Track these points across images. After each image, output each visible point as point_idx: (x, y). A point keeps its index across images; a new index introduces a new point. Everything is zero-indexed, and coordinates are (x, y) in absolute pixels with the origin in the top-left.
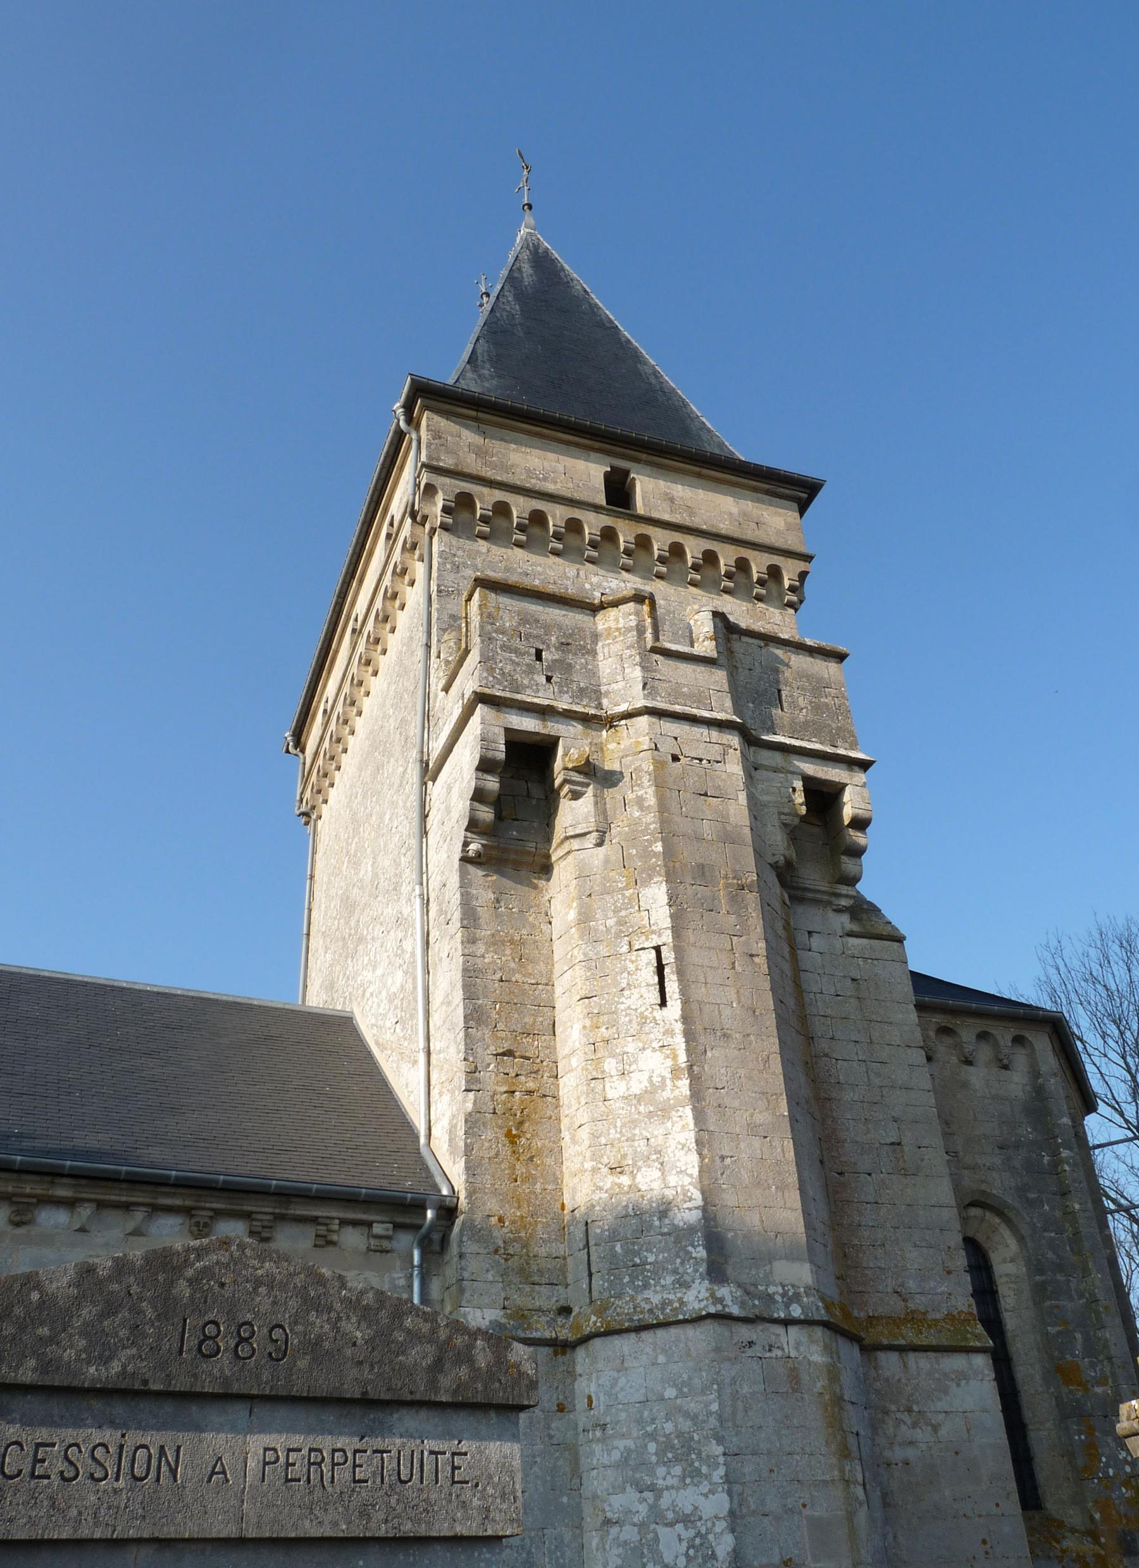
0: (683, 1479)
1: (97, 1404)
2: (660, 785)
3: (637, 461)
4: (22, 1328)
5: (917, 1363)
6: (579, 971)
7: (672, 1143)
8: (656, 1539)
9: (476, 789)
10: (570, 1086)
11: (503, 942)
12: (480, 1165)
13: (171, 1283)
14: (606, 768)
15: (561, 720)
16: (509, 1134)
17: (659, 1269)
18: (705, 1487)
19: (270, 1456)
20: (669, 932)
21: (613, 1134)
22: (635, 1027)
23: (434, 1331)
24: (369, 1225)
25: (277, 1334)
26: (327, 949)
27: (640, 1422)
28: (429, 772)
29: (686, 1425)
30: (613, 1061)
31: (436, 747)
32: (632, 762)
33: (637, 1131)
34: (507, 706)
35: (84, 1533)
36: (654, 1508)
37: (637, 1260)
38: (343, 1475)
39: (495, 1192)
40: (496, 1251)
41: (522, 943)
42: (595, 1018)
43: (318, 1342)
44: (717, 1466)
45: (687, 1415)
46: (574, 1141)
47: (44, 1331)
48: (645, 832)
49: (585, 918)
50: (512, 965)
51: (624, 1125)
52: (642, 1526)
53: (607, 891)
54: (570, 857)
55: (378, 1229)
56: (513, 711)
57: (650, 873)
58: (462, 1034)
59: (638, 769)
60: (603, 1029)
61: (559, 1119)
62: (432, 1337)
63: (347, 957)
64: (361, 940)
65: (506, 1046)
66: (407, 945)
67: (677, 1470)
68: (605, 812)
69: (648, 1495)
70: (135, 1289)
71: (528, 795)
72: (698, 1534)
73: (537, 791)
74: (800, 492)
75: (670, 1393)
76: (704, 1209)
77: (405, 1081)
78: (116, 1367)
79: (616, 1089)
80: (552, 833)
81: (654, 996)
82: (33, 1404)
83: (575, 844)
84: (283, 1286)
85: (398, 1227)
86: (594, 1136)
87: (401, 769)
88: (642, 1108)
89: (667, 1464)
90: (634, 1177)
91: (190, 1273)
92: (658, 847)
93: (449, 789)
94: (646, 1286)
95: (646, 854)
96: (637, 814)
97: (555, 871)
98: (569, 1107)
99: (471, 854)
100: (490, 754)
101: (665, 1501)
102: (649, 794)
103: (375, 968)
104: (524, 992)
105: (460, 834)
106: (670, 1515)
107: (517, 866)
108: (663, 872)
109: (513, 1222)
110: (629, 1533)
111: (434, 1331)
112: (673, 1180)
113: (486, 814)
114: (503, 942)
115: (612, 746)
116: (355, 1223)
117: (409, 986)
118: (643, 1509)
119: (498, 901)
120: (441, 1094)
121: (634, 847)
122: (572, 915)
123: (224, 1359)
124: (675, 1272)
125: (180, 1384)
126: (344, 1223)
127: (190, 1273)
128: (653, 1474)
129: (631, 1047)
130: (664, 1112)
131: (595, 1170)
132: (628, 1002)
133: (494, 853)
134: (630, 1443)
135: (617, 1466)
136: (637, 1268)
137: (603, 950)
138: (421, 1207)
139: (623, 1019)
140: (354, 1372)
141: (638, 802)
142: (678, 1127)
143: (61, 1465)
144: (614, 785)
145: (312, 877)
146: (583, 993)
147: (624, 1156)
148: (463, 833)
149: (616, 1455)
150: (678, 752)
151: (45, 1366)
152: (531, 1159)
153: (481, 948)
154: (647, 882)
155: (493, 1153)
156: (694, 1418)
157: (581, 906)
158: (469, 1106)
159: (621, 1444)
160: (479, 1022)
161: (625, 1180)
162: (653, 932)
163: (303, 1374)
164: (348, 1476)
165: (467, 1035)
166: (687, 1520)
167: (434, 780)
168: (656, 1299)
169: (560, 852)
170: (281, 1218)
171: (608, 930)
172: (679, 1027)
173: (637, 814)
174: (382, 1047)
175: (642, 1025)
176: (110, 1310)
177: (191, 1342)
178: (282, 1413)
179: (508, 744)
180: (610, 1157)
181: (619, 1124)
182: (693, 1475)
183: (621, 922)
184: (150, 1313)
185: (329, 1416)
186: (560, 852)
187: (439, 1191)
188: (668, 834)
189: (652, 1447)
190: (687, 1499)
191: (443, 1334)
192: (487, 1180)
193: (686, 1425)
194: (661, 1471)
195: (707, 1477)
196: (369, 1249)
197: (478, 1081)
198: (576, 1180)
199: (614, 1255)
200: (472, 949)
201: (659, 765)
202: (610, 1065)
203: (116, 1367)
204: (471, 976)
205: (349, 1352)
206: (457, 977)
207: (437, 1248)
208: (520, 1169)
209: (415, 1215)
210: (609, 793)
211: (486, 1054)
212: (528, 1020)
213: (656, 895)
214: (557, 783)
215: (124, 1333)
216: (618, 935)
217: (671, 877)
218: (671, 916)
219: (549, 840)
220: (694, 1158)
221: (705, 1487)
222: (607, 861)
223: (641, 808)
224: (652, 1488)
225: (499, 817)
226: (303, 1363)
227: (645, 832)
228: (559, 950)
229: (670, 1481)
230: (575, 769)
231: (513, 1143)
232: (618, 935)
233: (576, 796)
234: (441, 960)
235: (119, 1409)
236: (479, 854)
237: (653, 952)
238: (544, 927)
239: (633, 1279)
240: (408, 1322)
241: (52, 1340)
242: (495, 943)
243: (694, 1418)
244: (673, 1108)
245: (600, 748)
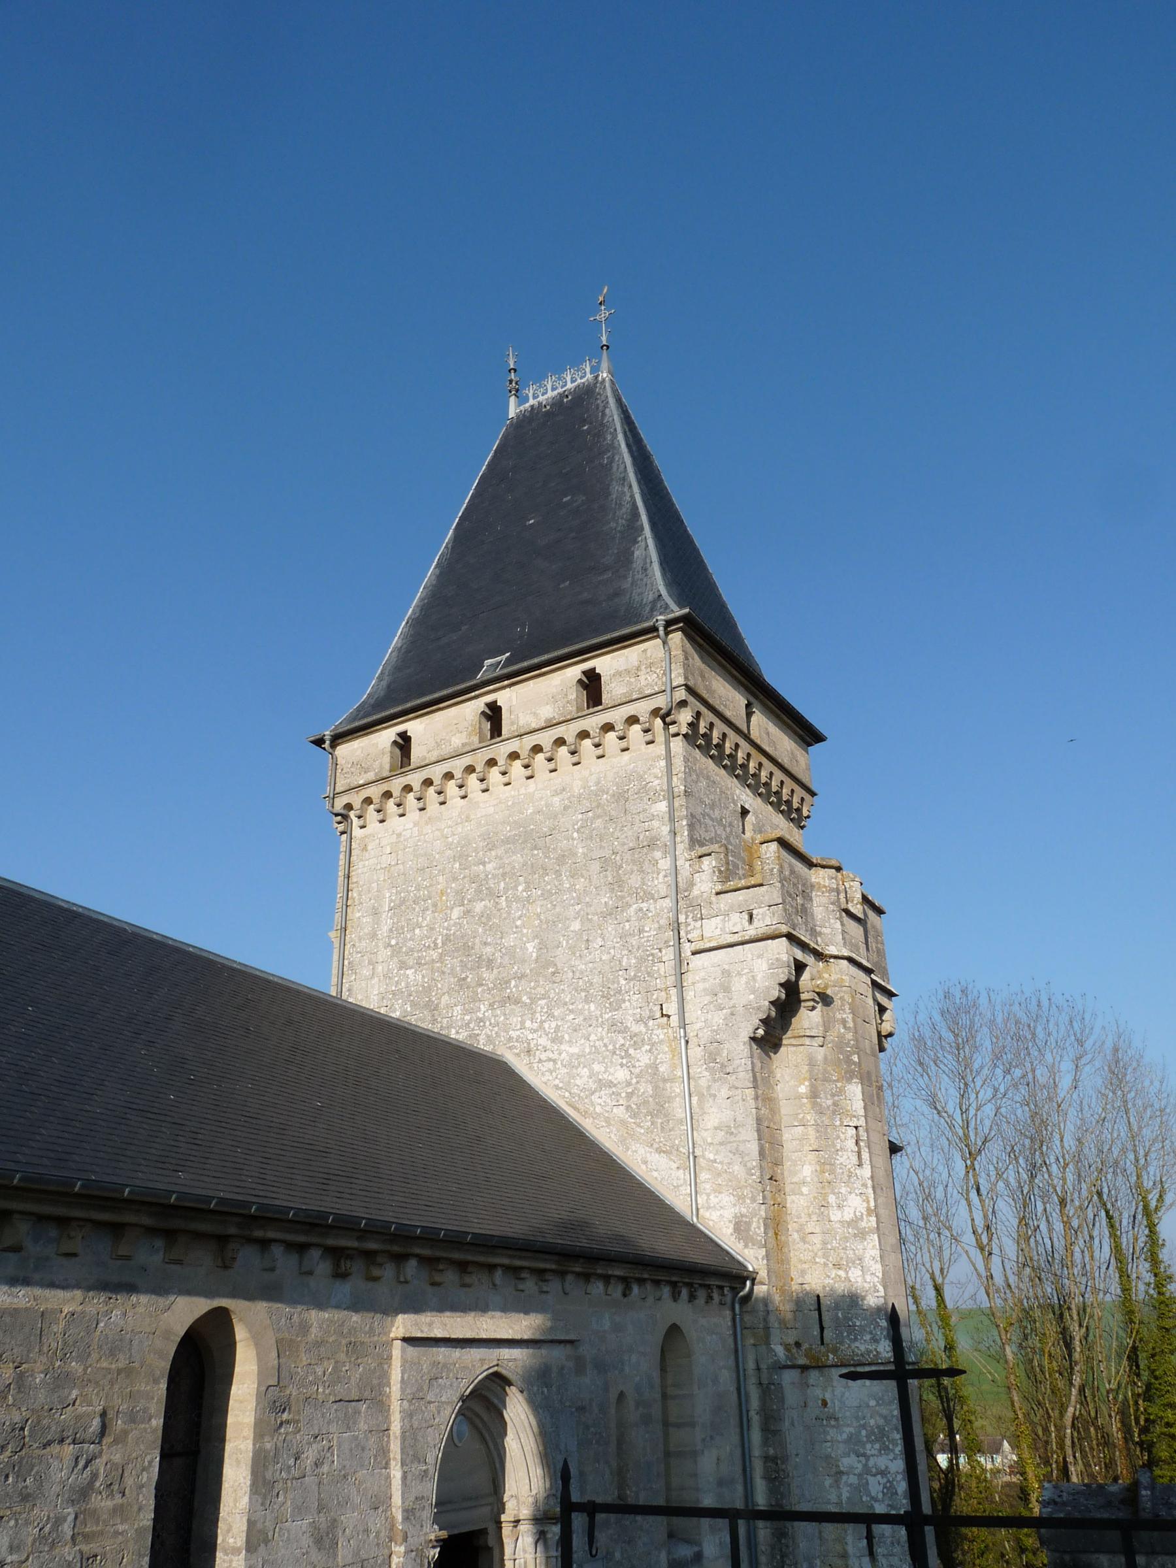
0: (880, 1451)
3: (761, 702)
5: (1109, 1465)
7: (867, 1255)
8: (867, 1483)
17: (863, 1329)
18: (891, 1456)
21: (834, 1244)
22: (845, 1178)
27: (857, 1418)
29: (881, 1422)
36: (865, 1465)
44: (897, 1445)
45: (881, 1416)
48: (848, 1045)
52: (860, 1476)
67: (877, 1446)
69: (862, 1459)
72: (888, 1481)
74: (808, 735)
75: (872, 1403)
76: (884, 1297)
79: (835, 1215)
81: (855, 1160)
83: (807, 1041)
86: (825, 1243)
89: (872, 1442)
90: (847, 1273)
94: (856, 1339)
97: (782, 1049)
101: (871, 1463)
106: (874, 1470)
110: (853, 1479)
112: (868, 1278)
118: (860, 1466)
124: (871, 1333)
128: (864, 1448)
130: (862, 1235)
131: (825, 1265)
132: (842, 1160)
134: (852, 1430)
135: (845, 1442)
136: (851, 1329)
142: (870, 1246)
146: (815, 1147)
149: (845, 1436)
154: (849, 1080)
156: (885, 1418)
159: (847, 1430)
161: (842, 1273)
166: (883, 1473)
168: (863, 1348)
169: (793, 1041)
172: (870, 1183)
175: (849, 1176)
182: (885, 1449)
183: (835, 1104)
189: (864, 1433)
190: (882, 1462)
193: (881, 1422)
194: (869, 1446)
195: (893, 1451)
199: (838, 1318)
202: (832, 1199)
220: (879, 1266)
221: (891, 1456)
223: (845, 1027)
224: (864, 1455)
227: (848, 1045)
229: (873, 1452)
239: (849, 1334)
243: (885, 1418)
244: (868, 1233)
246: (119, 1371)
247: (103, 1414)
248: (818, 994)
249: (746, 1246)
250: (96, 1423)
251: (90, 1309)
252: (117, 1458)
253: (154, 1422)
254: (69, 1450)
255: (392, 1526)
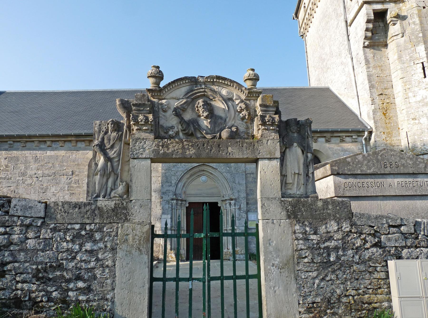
1: (370, 176)
2: (420, 17)
4: (356, 165)
6: (399, 72)
9: (366, 28)
10: (399, 100)
11: (377, 67)
12: (377, 121)
13: (377, 157)
14: (403, 15)
15: (388, 3)
16: (384, 113)
19: (398, 183)
20: (426, 58)
21: (413, 111)
22: (417, 84)
23: (424, 161)
24: (352, 136)
25: (396, 163)
26: (315, 71)
28: (348, 25)
30: (411, 93)
31: (350, 18)
32: (411, 12)
33: (419, 110)
34: (372, 3)
35: (372, 195)
37: (421, 139)
38: (411, 185)
39: (382, 127)
40: (384, 140)
41: (382, 66)
42: (405, 83)
43: (404, 164)
46: (401, 113)
47: (360, 166)
48: (416, 31)
49: (400, 57)
50: (380, 72)
51: (416, 108)
53: (405, 49)
54: (394, 41)
55: (354, 137)
56: (375, 4)
57: (419, 42)
58: (369, 91)
59: (413, 13)
60: (408, 86)
61: (396, 108)
62: (424, 162)
63: (324, 73)
64: (328, 68)
65: (381, 93)
66: (346, 69)
68: (403, 28)
70: (372, 158)
71: (379, 26)
73: (381, 24)
77: (352, 104)
78: (372, 170)
79: (412, 100)
80: (387, 35)
82: (360, 176)
83: (395, 38)
84: (396, 156)
85: (358, 136)
87: (336, 23)
88: (420, 104)
91: (380, 155)
92: (421, 35)
93: (356, 28)
95: (417, 37)
96: (413, 26)
97: (389, 45)
98: (399, 105)
99: (366, 45)
100: (369, 18)
102: (417, 21)
103: (335, 75)
104: (384, 79)
105: (363, 41)
107: (378, 46)
108: (423, 42)
109: (387, 133)
111: (424, 161)
113: (369, 34)
114: (377, 67)
115: (404, 8)
116: (348, 136)
117: (348, 80)
119: (374, 56)
120: (363, 105)
121: (413, 36)
122: (396, 57)
123: (389, 168)
125: (383, 172)
126: (346, 136)
127: (380, 155)
129: (416, 89)
131: (408, 120)
132: (414, 78)
133: (372, 44)
137: (406, 65)
138: (364, 132)
139: (413, 82)
140: (411, 169)
141: (414, 23)
143: (367, 185)
144: (405, 19)
145: (307, 52)
147: (416, 116)
148: (363, 40)
150: (424, 6)
151: (361, 171)
152: (390, 118)
153: (371, 69)
154: (418, 45)
155: (380, 118)
157: (398, 54)
158: (373, 108)
160: (373, 88)
162: (421, 59)
163: (402, 170)
164: (412, 185)
165: (370, 91)
167: (350, 26)
169: (391, 40)
170: (332, 137)
171: (407, 60)
173: (413, 26)
174: (341, 95)
176: (369, 162)
177: (383, 166)
178: (399, 176)
179: (374, 14)
180: (412, 116)
181: (414, 108)
183: (410, 57)
184: (375, 162)
185: (407, 176)
186: (391, 40)
187: (367, 128)
188: (423, 31)
191: (426, 162)
192: (380, 124)
196: (352, 141)
197: (374, 102)
198: (402, 122)
200: (369, 70)
201: (419, 11)
202: (410, 94)
203: (372, 170)
204: (369, 77)
205: (409, 166)
206: (366, 77)
207: (368, 140)
208: (387, 121)
209: (359, 132)
210: (404, 22)
211: (375, 95)
212: (386, 85)
213: (421, 49)
214: (388, 22)
215: (372, 165)
216: (410, 61)
217: (425, 43)
218: (426, 53)
219: (387, 37)
222: (405, 41)
223: (415, 24)
225: (372, 34)
226: (402, 168)
228: (392, 66)
230: (394, 17)
231: (385, 115)
232: (410, 61)
233: (394, 24)
234: (359, 73)
235: (373, 176)
236: (368, 45)
237: (421, 64)
238: (387, 61)
240: (419, 160)
241: (361, 167)
242: (375, 67)
245: (400, 9)
246: (75, 165)
247: (72, 171)
248: (394, 17)
249: (207, 117)
250: (71, 173)
251: (67, 155)
252: (77, 178)
253: (85, 173)
254: (65, 177)
255: (95, 190)
